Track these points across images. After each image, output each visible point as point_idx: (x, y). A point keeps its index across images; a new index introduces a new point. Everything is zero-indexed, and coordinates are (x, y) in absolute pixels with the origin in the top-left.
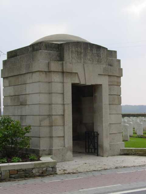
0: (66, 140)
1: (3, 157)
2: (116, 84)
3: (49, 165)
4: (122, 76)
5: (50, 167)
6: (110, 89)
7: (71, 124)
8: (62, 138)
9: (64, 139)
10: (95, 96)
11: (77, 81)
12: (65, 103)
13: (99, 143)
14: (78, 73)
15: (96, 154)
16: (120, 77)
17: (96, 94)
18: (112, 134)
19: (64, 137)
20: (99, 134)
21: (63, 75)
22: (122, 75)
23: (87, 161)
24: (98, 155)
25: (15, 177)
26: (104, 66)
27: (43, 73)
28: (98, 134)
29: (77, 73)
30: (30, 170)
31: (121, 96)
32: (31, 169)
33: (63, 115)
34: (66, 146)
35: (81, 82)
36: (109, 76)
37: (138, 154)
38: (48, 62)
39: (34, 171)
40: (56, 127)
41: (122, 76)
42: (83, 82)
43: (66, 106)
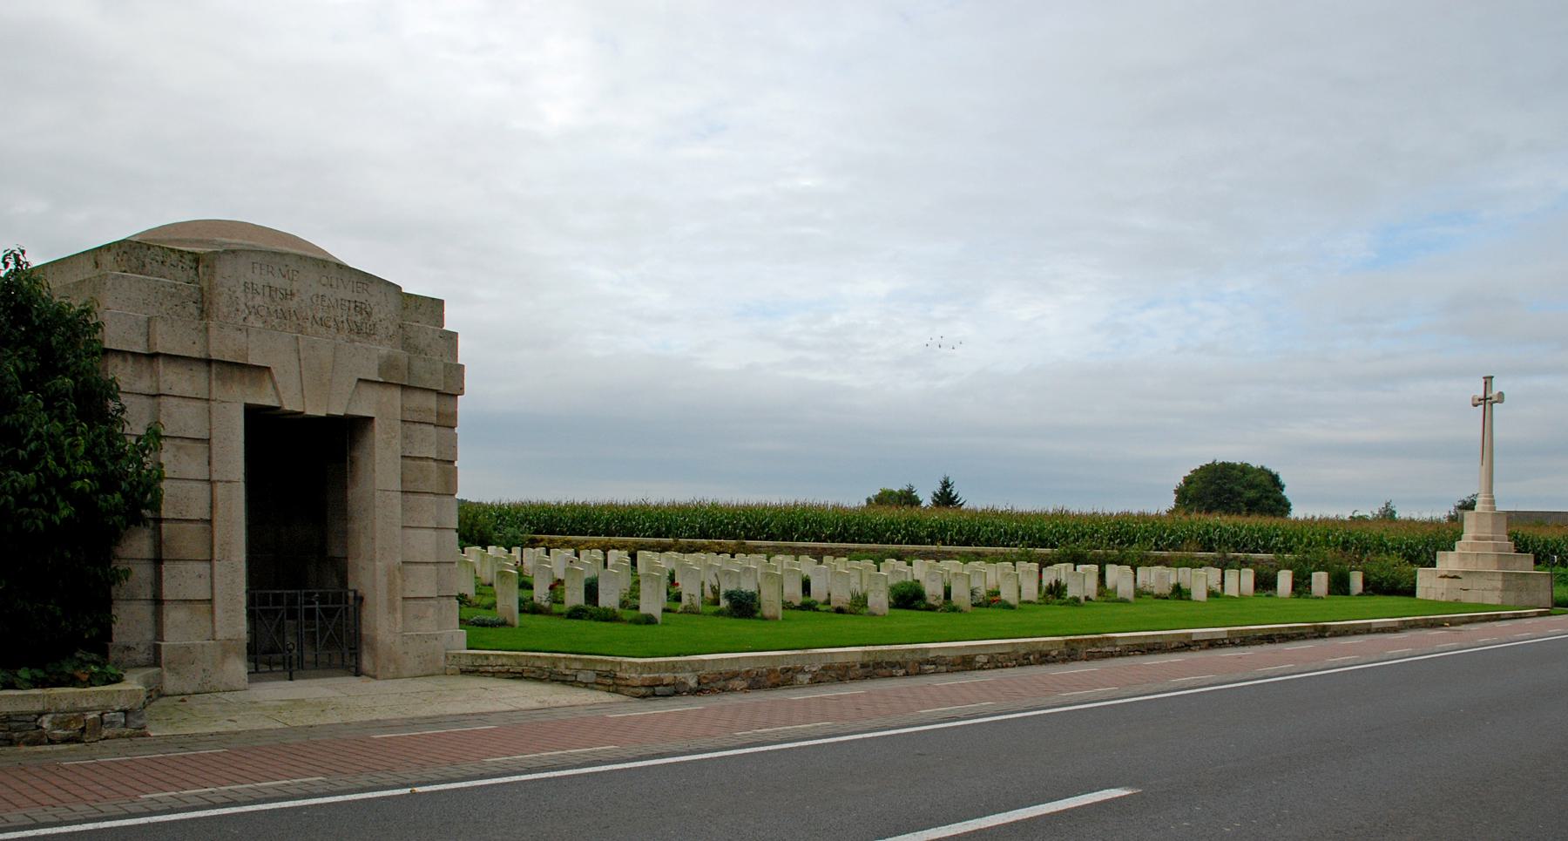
0: (218, 612)
1: (12, 665)
2: (434, 420)
3: (112, 703)
4: (461, 391)
5: (117, 708)
6: (406, 437)
7: (239, 556)
8: (205, 607)
9: (212, 612)
10: (351, 457)
11: (267, 399)
12: (215, 477)
13: (364, 632)
14: (273, 371)
15: (353, 669)
16: (457, 395)
17: (356, 454)
18: (415, 598)
19: (210, 601)
20: (362, 599)
21: (210, 372)
22: (462, 389)
23: (1366, 601)
24: (358, 673)
25: (587, 683)
26: (384, 350)
27: (125, 360)
28: (360, 599)
29: (269, 368)
30: (28, 718)
31: (456, 464)
32: (36, 713)
33: (210, 522)
34: (219, 636)
35: (284, 403)
36: (403, 387)
37: (508, 671)
38: (143, 317)
39: (46, 722)
40: (181, 566)
41: (462, 394)
42: (291, 404)
43: (220, 490)
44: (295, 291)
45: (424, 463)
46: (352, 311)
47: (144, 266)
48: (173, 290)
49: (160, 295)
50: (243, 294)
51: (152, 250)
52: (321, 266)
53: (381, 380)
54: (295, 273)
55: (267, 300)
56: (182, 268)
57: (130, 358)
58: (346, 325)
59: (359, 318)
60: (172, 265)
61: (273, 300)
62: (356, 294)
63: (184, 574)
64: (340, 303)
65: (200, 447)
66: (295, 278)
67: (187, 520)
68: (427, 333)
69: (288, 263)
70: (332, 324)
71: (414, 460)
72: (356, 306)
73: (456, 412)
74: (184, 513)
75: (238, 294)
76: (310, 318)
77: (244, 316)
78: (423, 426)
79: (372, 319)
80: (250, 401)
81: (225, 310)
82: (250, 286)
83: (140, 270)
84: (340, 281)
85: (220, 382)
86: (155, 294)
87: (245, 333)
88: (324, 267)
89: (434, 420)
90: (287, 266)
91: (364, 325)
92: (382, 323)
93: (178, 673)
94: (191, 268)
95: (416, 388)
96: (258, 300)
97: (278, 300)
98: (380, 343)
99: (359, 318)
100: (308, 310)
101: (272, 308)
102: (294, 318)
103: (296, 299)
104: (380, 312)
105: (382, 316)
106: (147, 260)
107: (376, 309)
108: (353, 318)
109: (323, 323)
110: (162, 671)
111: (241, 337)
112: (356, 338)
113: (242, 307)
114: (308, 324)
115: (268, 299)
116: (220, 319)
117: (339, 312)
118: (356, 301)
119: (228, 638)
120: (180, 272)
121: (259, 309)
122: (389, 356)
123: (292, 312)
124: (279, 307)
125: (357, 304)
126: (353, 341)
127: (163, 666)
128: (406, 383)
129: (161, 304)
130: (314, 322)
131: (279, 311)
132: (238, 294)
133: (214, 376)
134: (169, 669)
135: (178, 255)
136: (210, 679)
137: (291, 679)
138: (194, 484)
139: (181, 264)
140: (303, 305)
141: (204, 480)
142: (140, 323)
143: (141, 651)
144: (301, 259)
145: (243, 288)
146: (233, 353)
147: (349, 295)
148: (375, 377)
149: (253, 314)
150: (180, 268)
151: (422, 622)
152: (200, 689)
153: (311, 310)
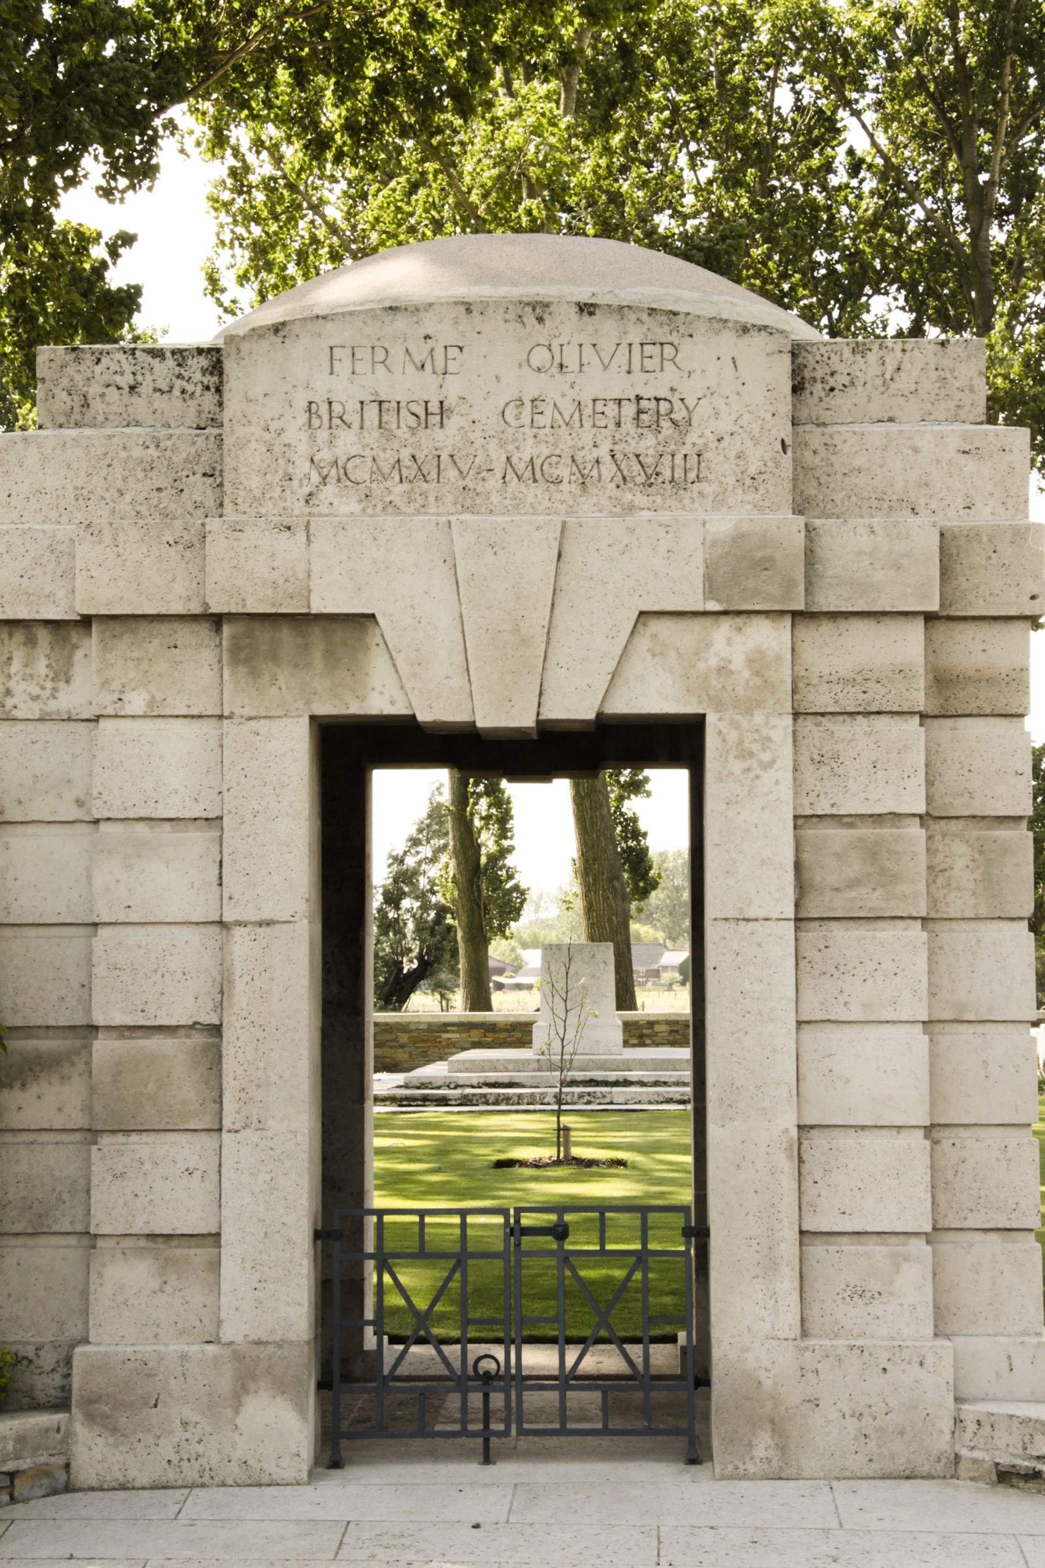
27: (31, 642)
29: (373, 616)
33: (216, 1030)
34: (228, 1333)
40: (141, 1146)
44: (451, 402)
45: (885, 832)
46: (628, 426)
47: (86, 405)
48: (153, 452)
49: (118, 471)
50: (304, 436)
51: (105, 361)
52: (530, 319)
53: (713, 606)
54: (453, 352)
55: (373, 436)
56: (183, 392)
57: (43, 636)
58: (608, 469)
59: (648, 444)
60: (156, 390)
61: (390, 436)
62: (638, 376)
63: (148, 1166)
64: (588, 411)
65: (199, 839)
66: (452, 367)
67: (160, 1029)
68: (916, 450)
69: (429, 331)
70: (564, 471)
71: (850, 826)
72: (640, 412)
73: (1025, 670)
74: (151, 1009)
75: (288, 437)
76: (499, 465)
77: (306, 490)
78: (881, 723)
79: (692, 438)
80: (326, 708)
81: (255, 482)
82: (324, 410)
83: (76, 416)
84: (588, 350)
85: (242, 670)
86: (104, 472)
87: (302, 537)
88: (540, 320)
89: (919, 699)
90: (427, 337)
91: (666, 460)
92: (725, 443)
93: (114, 1430)
94: (208, 388)
95: (965, 619)
96: (347, 442)
97: (403, 433)
98: (719, 501)
99: (648, 444)
100: (492, 446)
101: (386, 460)
102: (452, 474)
103: (453, 423)
104: (717, 415)
105: (724, 425)
106: (94, 390)
107: (703, 410)
108: (633, 446)
109: (535, 472)
110: (70, 1422)
111: (291, 546)
112: (640, 500)
113: (304, 466)
114: (493, 482)
115: (376, 434)
116: (241, 508)
117: (587, 435)
118: (639, 398)
119: (254, 1337)
120: (179, 403)
121: (350, 465)
122: (738, 538)
123: (445, 458)
124: (405, 454)
125: (644, 404)
126: (630, 509)
127: (74, 1410)
128: (801, 606)
129: (121, 493)
130: (511, 475)
131: (407, 462)
132: (288, 437)
133: (225, 658)
134: (90, 1418)
135: (170, 362)
136: (200, 1448)
137: (487, 1459)
138: (185, 932)
139: (178, 384)
140: (476, 436)
141: (213, 922)
142: (60, 548)
143: (47, 1367)
144: (469, 311)
145: (303, 418)
146: (270, 592)
147: (618, 385)
148: (697, 604)
149: (332, 481)
150: (176, 392)
151: (877, 1308)
152: (171, 1475)
153: (502, 443)
